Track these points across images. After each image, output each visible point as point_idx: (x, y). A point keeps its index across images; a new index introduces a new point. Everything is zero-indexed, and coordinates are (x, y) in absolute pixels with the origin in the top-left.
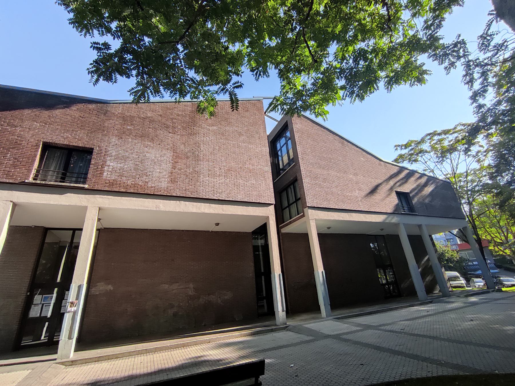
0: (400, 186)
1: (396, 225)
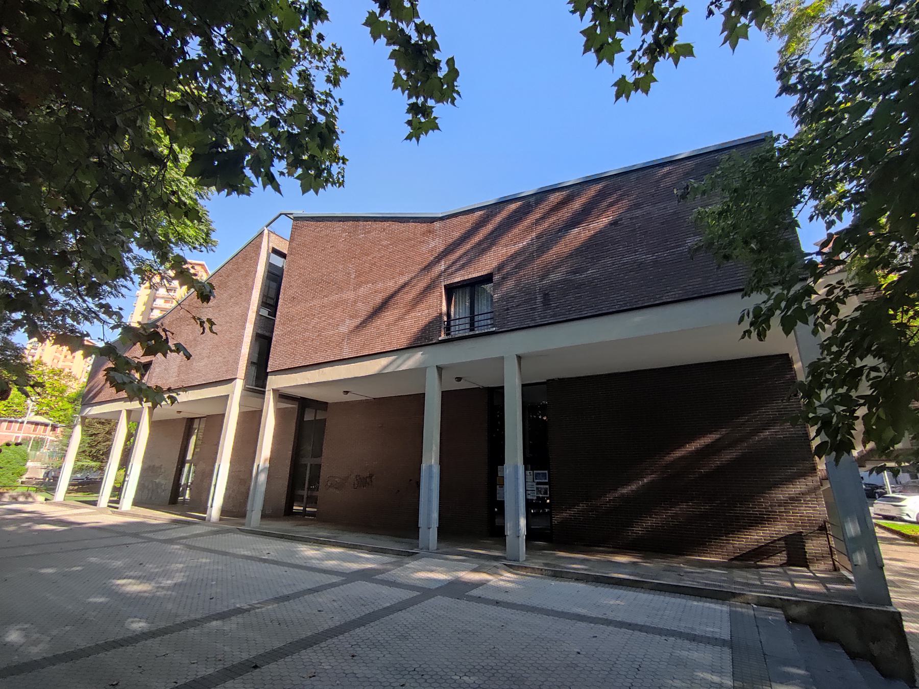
0: (463, 267)
1: (419, 372)
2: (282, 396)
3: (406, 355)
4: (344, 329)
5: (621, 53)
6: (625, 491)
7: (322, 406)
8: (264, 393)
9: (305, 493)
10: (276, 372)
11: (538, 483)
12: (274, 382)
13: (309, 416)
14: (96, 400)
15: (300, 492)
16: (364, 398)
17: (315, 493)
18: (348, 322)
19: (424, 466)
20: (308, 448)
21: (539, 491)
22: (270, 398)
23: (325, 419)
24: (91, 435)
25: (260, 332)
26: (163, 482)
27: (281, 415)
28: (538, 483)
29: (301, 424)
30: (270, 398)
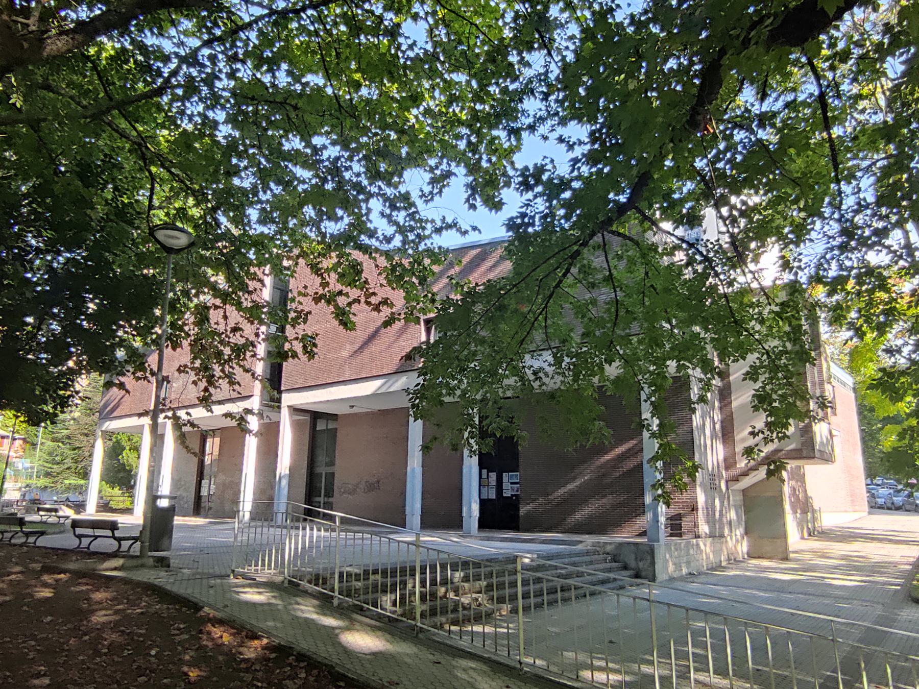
2: (295, 410)
3: (395, 377)
4: (345, 353)
5: (338, 435)
6: (571, 486)
7: (333, 417)
8: (279, 407)
9: (321, 499)
10: (288, 391)
11: (512, 483)
12: (289, 399)
13: (321, 426)
14: (115, 414)
15: (317, 499)
16: (364, 410)
17: (331, 500)
18: (348, 347)
19: (409, 468)
20: (321, 458)
21: (512, 489)
22: (285, 414)
23: (336, 429)
24: (74, 449)
25: (270, 349)
26: (185, 494)
27: (296, 425)
28: (512, 483)
29: (314, 434)
30: (285, 414)
